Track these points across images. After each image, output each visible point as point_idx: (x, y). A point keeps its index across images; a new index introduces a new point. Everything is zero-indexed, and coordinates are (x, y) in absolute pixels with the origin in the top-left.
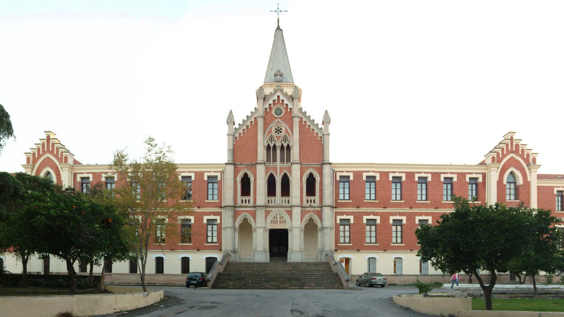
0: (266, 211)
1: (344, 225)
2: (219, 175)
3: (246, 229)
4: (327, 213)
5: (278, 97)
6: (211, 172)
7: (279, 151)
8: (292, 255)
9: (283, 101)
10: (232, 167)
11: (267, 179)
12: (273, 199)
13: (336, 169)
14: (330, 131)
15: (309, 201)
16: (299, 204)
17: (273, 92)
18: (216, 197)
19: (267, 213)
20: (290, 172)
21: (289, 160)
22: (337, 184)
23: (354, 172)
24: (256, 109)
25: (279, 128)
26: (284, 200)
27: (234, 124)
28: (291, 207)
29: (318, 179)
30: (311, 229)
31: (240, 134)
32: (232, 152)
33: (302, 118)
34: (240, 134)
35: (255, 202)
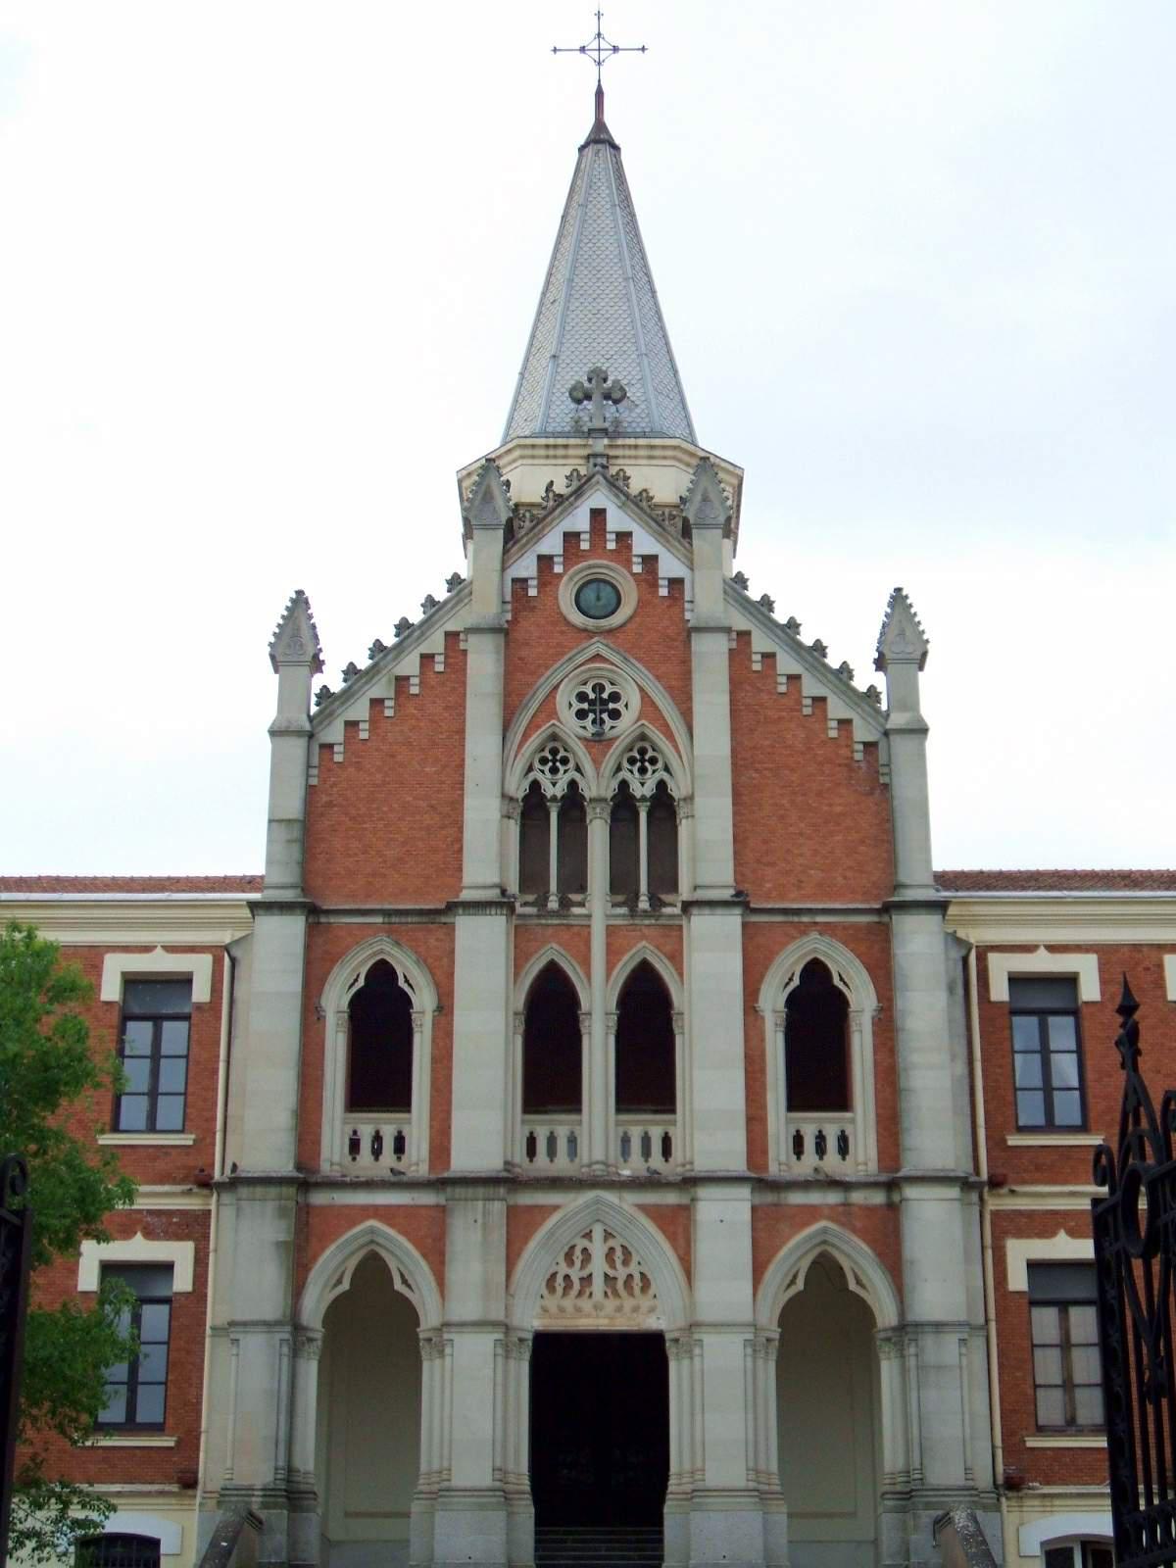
0: (512, 1212)
1: (1063, 1306)
2: (200, 967)
3: (370, 1341)
4: (935, 1224)
5: (598, 515)
6: (147, 949)
7: (598, 830)
8: (440, 1517)
9: (624, 537)
10: (294, 927)
11: (520, 1002)
12: (562, 1134)
13: (976, 936)
14: (928, 710)
15: (809, 1144)
16: (738, 1164)
17: (560, 487)
18: (170, 1111)
19: (520, 1227)
20: (676, 958)
21: (665, 878)
22: (996, 1021)
23: (1106, 953)
24: (455, 582)
25: (599, 688)
26: (636, 1134)
27: (317, 665)
28: (690, 1182)
29: (862, 999)
30: (827, 1339)
31: (352, 725)
32: (296, 833)
33: (744, 636)
34: (352, 725)
35: (440, 1148)
